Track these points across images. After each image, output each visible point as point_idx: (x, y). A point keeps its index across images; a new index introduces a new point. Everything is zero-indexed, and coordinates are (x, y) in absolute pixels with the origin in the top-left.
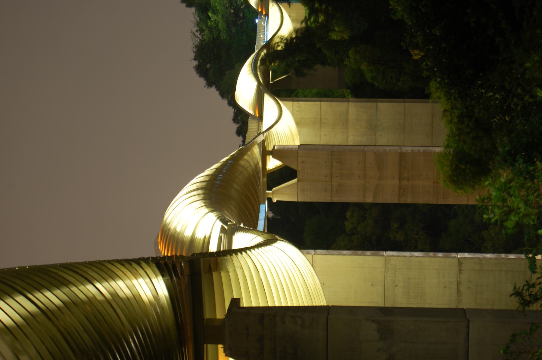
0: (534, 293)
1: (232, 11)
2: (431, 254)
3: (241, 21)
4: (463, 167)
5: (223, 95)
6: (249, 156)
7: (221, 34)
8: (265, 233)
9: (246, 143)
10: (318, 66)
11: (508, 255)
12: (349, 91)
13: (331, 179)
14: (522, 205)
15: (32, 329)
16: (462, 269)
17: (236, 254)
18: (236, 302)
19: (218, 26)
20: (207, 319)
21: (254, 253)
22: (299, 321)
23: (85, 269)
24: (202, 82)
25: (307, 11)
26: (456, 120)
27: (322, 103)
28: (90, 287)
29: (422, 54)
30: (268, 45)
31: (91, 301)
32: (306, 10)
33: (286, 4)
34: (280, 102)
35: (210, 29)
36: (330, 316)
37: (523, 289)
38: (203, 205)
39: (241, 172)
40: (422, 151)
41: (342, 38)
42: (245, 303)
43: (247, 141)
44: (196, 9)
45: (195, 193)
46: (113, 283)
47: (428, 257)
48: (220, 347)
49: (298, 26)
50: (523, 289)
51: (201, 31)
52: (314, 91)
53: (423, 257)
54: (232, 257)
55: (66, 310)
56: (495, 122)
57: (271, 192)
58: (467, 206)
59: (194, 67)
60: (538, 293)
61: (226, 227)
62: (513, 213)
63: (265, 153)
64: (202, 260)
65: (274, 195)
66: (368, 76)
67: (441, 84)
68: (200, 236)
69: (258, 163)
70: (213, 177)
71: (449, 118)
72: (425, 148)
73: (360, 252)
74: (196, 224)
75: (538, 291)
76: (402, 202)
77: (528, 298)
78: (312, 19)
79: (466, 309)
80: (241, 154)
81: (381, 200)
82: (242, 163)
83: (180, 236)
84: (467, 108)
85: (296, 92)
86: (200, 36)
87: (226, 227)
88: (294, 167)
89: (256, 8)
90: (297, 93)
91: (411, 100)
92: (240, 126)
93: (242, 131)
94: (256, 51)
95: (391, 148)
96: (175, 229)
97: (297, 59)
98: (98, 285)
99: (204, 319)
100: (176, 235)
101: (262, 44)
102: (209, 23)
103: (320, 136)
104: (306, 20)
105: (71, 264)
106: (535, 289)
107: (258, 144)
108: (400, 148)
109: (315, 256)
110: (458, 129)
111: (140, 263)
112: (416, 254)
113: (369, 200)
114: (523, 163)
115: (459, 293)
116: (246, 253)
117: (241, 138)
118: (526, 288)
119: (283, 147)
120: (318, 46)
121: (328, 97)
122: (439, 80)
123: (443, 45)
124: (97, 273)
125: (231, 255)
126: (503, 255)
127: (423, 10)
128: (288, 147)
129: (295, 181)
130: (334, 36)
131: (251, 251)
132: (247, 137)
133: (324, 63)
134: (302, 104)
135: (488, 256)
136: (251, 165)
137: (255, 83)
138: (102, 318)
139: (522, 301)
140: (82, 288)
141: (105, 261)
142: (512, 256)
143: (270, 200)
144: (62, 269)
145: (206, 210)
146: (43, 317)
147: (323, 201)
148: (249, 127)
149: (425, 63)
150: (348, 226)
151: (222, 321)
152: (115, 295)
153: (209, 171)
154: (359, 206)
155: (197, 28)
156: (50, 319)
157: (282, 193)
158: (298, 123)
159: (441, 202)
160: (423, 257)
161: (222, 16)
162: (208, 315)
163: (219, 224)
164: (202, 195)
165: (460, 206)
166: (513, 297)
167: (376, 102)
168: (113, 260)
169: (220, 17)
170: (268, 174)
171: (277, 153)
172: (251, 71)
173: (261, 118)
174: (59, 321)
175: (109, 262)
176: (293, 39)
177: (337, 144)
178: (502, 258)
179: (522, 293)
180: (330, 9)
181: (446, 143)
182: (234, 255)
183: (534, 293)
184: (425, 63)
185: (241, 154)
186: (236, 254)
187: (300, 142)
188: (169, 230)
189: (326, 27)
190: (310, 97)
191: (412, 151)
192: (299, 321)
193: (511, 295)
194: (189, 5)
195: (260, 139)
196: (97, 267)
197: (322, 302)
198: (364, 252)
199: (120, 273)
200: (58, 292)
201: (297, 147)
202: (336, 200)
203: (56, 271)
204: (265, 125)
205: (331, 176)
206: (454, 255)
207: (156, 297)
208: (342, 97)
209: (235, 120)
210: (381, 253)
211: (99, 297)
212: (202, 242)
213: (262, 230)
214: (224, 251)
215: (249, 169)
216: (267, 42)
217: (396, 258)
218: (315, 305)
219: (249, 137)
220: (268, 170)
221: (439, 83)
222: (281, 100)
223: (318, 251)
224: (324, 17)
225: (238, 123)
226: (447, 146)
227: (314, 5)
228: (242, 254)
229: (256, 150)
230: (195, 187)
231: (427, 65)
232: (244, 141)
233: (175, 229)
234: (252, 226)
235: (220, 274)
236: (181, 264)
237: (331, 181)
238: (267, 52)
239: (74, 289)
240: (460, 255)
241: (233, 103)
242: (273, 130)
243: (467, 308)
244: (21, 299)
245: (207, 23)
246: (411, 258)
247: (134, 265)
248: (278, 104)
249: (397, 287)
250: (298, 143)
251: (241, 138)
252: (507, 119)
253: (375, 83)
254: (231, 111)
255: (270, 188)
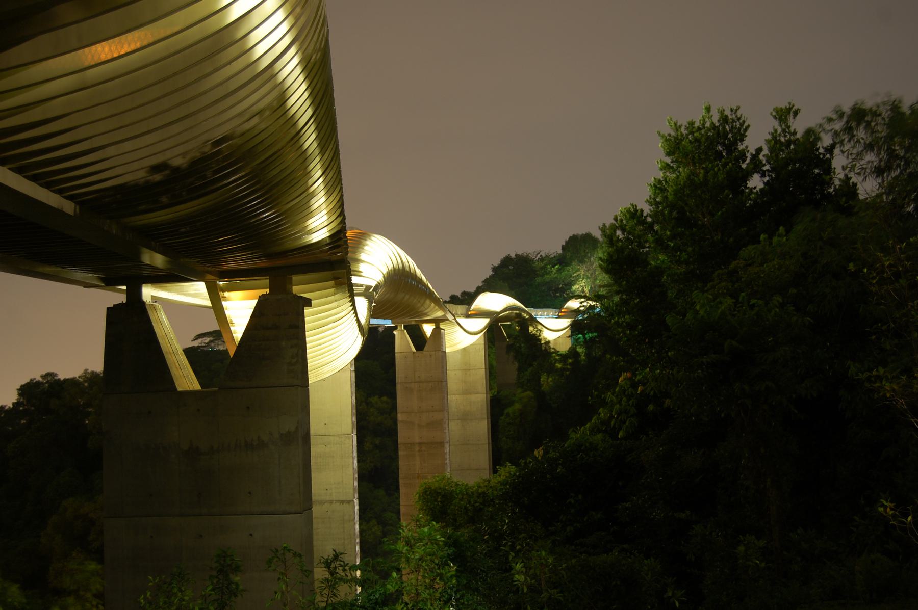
0: (337, 571)
1: (561, 286)
2: (356, 476)
3: (552, 295)
4: (439, 500)
5: (485, 281)
6: (434, 307)
7: (540, 278)
8: (368, 326)
9: (445, 304)
10: (517, 365)
11: (359, 544)
12: (496, 393)
13: (417, 382)
14: (417, 556)
15: (283, 124)
16: (344, 504)
17: (350, 301)
18: (308, 302)
19: (547, 274)
20: (292, 278)
21: (352, 316)
22: (294, 360)
23: (335, 168)
24: (497, 262)
25: (564, 353)
26: (480, 491)
27: (484, 370)
28: (319, 173)
29: (540, 458)
30: (533, 320)
31: (307, 174)
32: (565, 351)
33: (570, 333)
34: (483, 333)
35: (544, 267)
36: (299, 388)
37: (341, 561)
38: (390, 269)
39: (419, 301)
40: (446, 462)
41: (543, 385)
42: (307, 311)
43: (447, 305)
44: (560, 254)
45: (399, 261)
46: (323, 193)
47: (354, 474)
48: (268, 291)
49: (552, 345)
50: (341, 561)
51: (542, 259)
52: (494, 363)
53: (353, 468)
54: (348, 297)
55: (300, 152)
56: (483, 526)
57: (403, 328)
58: (399, 505)
59: (509, 255)
60: (338, 575)
61: (371, 291)
62: (409, 549)
63: (437, 321)
64: (345, 271)
65: (400, 332)
66: (510, 410)
67: (514, 476)
68: (362, 267)
69: (428, 316)
70: (414, 276)
71: (482, 485)
72: (448, 464)
73: (355, 411)
74: (373, 264)
75: (340, 575)
76: (399, 446)
77: (333, 565)
78: (557, 358)
79: (312, 511)
80: (436, 300)
81: (400, 427)
82: (428, 302)
83: (360, 250)
84: (492, 500)
85: (492, 346)
86: (537, 258)
87: (371, 291)
88: (426, 348)
89: (565, 307)
90: (491, 347)
91: (491, 449)
92: (459, 298)
93: (454, 300)
94: (526, 309)
95: (447, 434)
96: (367, 245)
97: (523, 345)
98: (321, 180)
99: (291, 275)
100: (361, 246)
101: (533, 314)
102: (549, 266)
103: (454, 370)
104: (556, 352)
105: (338, 155)
106: (342, 572)
107: (445, 315)
108: (447, 442)
109: (350, 372)
110: (472, 493)
111: (340, 216)
112: (356, 462)
113: (400, 417)
114: (448, 553)
115: (322, 502)
116: (352, 310)
117: (448, 299)
118: (342, 563)
119: (443, 338)
120: (535, 363)
121: (490, 376)
122: (517, 474)
123: (548, 476)
124: (331, 179)
125: (350, 296)
126: (358, 540)
127: (579, 456)
128: (444, 342)
129: (414, 350)
130: (543, 378)
131: (353, 314)
132: (450, 305)
133: (520, 370)
134: (482, 353)
135: (357, 527)
136: (426, 309)
137: (499, 310)
138: (293, 184)
139: (329, 561)
140: (319, 166)
141: (342, 184)
142: (358, 548)
143: (395, 328)
144: (334, 147)
145: (385, 271)
146: (293, 132)
147: (397, 375)
148: (459, 306)
149: (531, 460)
150: (374, 399)
151: (291, 292)
152: (312, 195)
153: (419, 272)
154: (394, 407)
155: (544, 256)
156: (292, 139)
157: (401, 338)
158: (465, 350)
159: (401, 481)
160: (353, 468)
161: (556, 278)
162: (295, 278)
163: (373, 284)
164: (398, 267)
165: (398, 498)
166: (334, 553)
167: (488, 419)
168: (342, 192)
169: (556, 275)
170: (418, 325)
171: (437, 332)
172: (509, 305)
173: (468, 316)
174: (291, 146)
175: (341, 188)
176: (540, 342)
177: (448, 386)
178: (355, 540)
179: (337, 561)
180: (568, 373)
181: (460, 484)
182: (350, 299)
183: (337, 571)
184: (531, 460)
185: (436, 300)
186: (350, 301)
187: (448, 353)
188: (366, 240)
189: (551, 370)
190: (489, 359)
191: (446, 453)
192: (294, 360)
193: (334, 551)
194: (564, 248)
195: (450, 317)
196: (337, 177)
197: (312, 379)
198: (355, 416)
199: (331, 198)
200: (315, 145)
201: (444, 350)
202: (398, 387)
203: (333, 142)
204: (462, 320)
205: (420, 382)
206: (357, 496)
207: (311, 232)
208: (490, 387)
209: (464, 293)
210: (355, 431)
211: (311, 182)
212: (357, 269)
213: (371, 323)
214: (353, 290)
215: (422, 308)
216: (536, 318)
217: (351, 444)
218: (309, 373)
219: (451, 307)
220: (423, 325)
221: (515, 475)
222: (484, 333)
223: (354, 374)
224: (561, 368)
225: (461, 296)
226: (457, 485)
227: (570, 358)
228: (351, 306)
229: (439, 314)
230: (405, 260)
231: (530, 462)
232: (445, 302)
233: (367, 245)
234: (374, 313)
235: (333, 287)
236: (340, 253)
237: (415, 382)
238: (527, 318)
239: (318, 159)
240: (356, 501)
241: (480, 291)
242: (458, 327)
243: (313, 512)
244: (310, 112)
245: (549, 264)
246: (352, 457)
247: (339, 211)
248: (482, 332)
249: (324, 447)
250: (448, 350)
251: (448, 299)
252: (486, 537)
253: (504, 416)
254: (472, 290)
255: (405, 327)
